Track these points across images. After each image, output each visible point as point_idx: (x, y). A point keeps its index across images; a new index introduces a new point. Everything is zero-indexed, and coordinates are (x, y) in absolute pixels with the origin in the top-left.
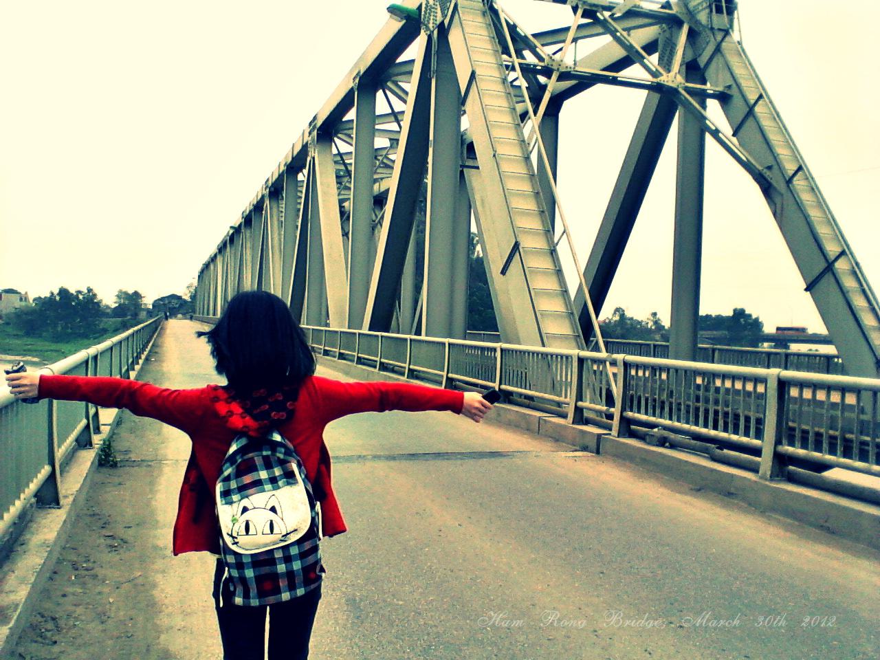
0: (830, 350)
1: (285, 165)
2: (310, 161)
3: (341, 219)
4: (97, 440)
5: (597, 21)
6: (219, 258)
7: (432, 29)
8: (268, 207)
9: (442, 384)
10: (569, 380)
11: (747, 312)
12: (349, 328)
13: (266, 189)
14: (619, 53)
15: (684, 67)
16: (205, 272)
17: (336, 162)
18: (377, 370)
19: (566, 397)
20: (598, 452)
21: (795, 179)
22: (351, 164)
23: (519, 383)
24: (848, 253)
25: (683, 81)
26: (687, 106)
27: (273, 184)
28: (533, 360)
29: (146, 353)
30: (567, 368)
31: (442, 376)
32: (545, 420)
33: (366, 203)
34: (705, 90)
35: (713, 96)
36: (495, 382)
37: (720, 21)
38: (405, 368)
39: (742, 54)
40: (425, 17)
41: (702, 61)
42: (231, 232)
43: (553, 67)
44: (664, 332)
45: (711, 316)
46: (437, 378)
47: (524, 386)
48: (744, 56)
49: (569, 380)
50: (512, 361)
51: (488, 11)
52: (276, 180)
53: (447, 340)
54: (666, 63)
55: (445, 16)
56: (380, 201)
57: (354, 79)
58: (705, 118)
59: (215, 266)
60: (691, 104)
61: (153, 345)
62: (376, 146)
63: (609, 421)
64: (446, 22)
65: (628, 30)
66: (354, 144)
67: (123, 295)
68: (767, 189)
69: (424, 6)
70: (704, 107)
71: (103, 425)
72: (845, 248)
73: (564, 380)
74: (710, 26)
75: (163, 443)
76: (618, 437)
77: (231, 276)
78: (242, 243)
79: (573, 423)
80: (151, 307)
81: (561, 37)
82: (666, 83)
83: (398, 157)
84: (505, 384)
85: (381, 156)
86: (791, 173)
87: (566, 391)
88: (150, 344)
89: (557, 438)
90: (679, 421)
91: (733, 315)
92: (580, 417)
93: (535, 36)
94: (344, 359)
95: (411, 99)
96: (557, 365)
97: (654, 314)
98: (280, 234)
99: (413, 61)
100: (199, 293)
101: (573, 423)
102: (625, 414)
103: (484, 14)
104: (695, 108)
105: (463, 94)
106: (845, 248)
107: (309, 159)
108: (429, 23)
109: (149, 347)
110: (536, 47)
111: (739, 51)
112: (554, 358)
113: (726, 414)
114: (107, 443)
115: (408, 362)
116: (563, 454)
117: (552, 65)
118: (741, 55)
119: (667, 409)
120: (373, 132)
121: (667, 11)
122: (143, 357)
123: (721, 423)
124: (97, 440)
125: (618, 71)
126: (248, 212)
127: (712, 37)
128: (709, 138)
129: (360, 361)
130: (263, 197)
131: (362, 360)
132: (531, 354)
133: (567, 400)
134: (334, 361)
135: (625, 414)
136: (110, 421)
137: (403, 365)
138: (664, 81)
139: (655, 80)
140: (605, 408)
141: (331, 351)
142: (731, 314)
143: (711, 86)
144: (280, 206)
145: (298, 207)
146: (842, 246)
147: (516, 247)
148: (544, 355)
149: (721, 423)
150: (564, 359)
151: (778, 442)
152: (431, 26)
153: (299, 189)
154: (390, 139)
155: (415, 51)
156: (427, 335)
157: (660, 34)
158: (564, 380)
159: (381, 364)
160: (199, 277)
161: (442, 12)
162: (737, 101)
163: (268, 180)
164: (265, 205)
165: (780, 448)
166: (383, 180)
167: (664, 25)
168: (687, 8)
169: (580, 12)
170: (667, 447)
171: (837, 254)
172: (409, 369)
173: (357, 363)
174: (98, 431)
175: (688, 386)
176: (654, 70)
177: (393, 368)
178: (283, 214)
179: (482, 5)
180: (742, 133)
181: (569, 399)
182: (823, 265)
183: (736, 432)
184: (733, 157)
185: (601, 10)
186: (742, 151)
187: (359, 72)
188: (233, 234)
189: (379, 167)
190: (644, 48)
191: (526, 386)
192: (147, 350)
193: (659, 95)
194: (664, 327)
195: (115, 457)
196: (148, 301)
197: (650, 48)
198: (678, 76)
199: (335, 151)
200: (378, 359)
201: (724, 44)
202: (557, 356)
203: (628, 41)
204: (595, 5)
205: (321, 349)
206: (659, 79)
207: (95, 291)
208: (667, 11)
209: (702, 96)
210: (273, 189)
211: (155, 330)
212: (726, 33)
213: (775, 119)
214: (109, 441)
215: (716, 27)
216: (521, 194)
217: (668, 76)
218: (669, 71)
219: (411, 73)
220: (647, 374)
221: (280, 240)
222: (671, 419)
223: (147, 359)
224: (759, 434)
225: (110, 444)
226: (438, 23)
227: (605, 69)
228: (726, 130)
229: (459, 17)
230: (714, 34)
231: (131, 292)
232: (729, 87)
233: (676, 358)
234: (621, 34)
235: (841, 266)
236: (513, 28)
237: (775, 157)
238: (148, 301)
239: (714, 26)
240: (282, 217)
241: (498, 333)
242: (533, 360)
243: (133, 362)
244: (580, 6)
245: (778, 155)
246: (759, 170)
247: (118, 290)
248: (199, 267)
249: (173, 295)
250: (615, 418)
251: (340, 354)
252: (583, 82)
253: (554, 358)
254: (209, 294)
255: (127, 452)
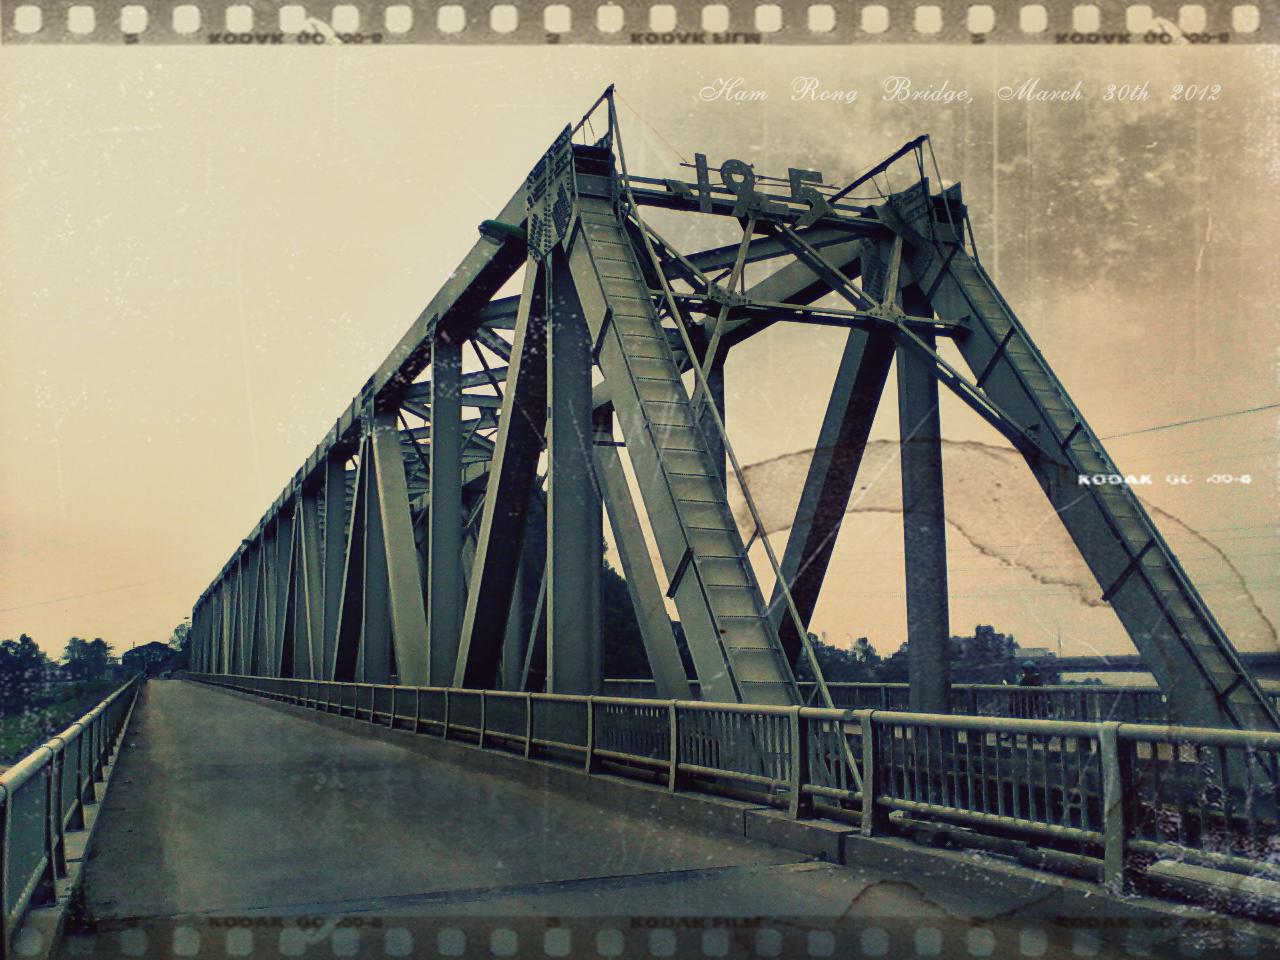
0: (1144, 680)
2: (365, 443)
4: (64, 888)
5: (774, 235)
7: (544, 253)
8: (301, 509)
10: (786, 750)
11: (996, 631)
12: (432, 685)
13: (297, 484)
14: (806, 277)
15: (900, 295)
19: (783, 778)
20: (842, 860)
21: (1072, 442)
22: (428, 445)
25: (903, 314)
26: (910, 346)
27: (307, 477)
29: (121, 735)
30: (782, 733)
32: (755, 816)
33: (454, 498)
36: (669, 759)
37: (943, 232)
41: (926, 286)
42: (245, 547)
43: (719, 301)
46: (577, 757)
47: (715, 764)
49: (786, 750)
50: (538, 707)
51: (624, 229)
52: (1014, 444)
54: (875, 287)
55: (562, 235)
56: (472, 493)
57: (429, 325)
58: (934, 360)
59: (220, 600)
60: (916, 344)
61: (130, 722)
62: (465, 417)
63: (857, 812)
64: (565, 245)
65: (817, 247)
67: (77, 645)
68: (1036, 459)
69: (530, 222)
70: (934, 347)
71: (69, 861)
73: (778, 751)
74: (931, 239)
76: (872, 835)
77: (244, 613)
78: (262, 566)
79: (798, 818)
80: (120, 662)
81: (728, 259)
82: (878, 317)
83: (497, 436)
84: (685, 762)
86: (1066, 434)
88: (127, 722)
89: (776, 842)
92: (808, 809)
94: (427, 732)
97: (864, 641)
98: (319, 550)
99: (517, 299)
101: (798, 818)
102: (879, 800)
103: (618, 231)
107: (362, 440)
108: (539, 246)
110: (693, 273)
111: (975, 270)
112: (761, 720)
113: (1008, 787)
115: (590, 744)
116: (792, 868)
117: (718, 298)
118: (979, 277)
119: (944, 790)
120: (462, 400)
121: (871, 220)
122: (119, 742)
124: (64, 888)
127: (936, 252)
128: (943, 389)
130: (293, 495)
131: (604, 762)
132: (730, 715)
134: (411, 736)
135: (879, 800)
136: (80, 853)
137: (523, 738)
138: (876, 314)
139: (863, 313)
140: (846, 792)
141: (405, 720)
142: (972, 634)
143: (940, 317)
145: (348, 508)
146: (1149, 534)
147: (689, 555)
148: (746, 716)
150: (768, 719)
151: (1128, 834)
152: (542, 249)
153: (348, 482)
154: (481, 409)
155: (517, 284)
156: (555, 692)
157: (861, 251)
158: (778, 751)
160: (194, 615)
161: (558, 230)
162: (979, 336)
163: (300, 472)
164: (296, 508)
165: (1133, 844)
167: (867, 239)
168: (899, 217)
169: (751, 225)
170: (948, 848)
171: (1144, 545)
174: (62, 873)
175: (947, 746)
176: (858, 296)
177: (504, 744)
178: (325, 520)
180: (988, 382)
181: (787, 780)
182: (1126, 561)
187: (437, 315)
188: (247, 551)
189: (467, 447)
190: (842, 269)
192: (123, 731)
194: (879, 657)
195: (92, 917)
197: (852, 270)
198: (895, 307)
199: (401, 427)
201: (953, 262)
203: (821, 261)
204: (773, 216)
205: (389, 718)
206: (869, 312)
207: (35, 640)
208: (871, 220)
209: (929, 333)
210: (307, 484)
211: (130, 701)
212: (957, 246)
213: (1035, 360)
215: (941, 240)
216: (690, 480)
217: (881, 308)
219: (514, 314)
221: (320, 556)
222: (952, 804)
223: (124, 745)
225: (82, 893)
226: (552, 245)
227: (788, 301)
228: (969, 376)
229: (584, 235)
230: (938, 249)
231: (90, 640)
232: (967, 319)
233: (921, 711)
235: (1150, 561)
236: (661, 248)
237: (1043, 414)
243: (105, 751)
244: (750, 217)
246: (1021, 432)
247: (70, 637)
251: (419, 724)
252: (751, 320)
253: (761, 720)
255: (108, 905)
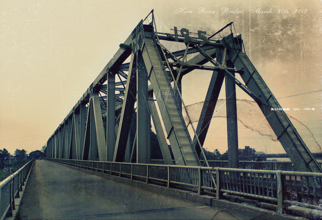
0: (287, 160)
1: (81, 102)
2: (90, 100)
3: (103, 120)
4: (14, 212)
6: (55, 136)
9: (146, 181)
10: (197, 178)
11: (250, 148)
12: (107, 161)
14: (202, 58)
16: (50, 142)
17: (100, 100)
18: (131, 180)
19: (196, 185)
21: (269, 100)
22: (106, 101)
23: (177, 180)
24: (291, 125)
27: (76, 108)
28: (182, 171)
29: (29, 174)
30: (196, 173)
31: (119, 173)
34: (234, 70)
35: (237, 72)
36: (168, 180)
37: (237, 47)
38: (131, 176)
39: (246, 57)
40: (133, 48)
42: (60, 126)
44: (221, 156)
45: (254, 151)
46: (144, 179)
48: (247, 58)
49: (197, 178)
53: (147, 164)
54: (220, 60)
55: (140, 47)
56: (118, 112)
57: (107, 70)
58: (235, 79)
59: (54, 139)
60: (230, 75)
61: (31, 170)
62: (116, 93)
64: (141, 50)
65: (205, 50)
66: (107, 93)
69: (132, 44)
70: (235, 76)
72: (290, 123)
73: (195, 178)
74: (234, 48)
75: (40, 211)
76: (219, 199)
79: (200, 194)
80: (29, 155)
81: (182, 53)
82: (220, 68)
83: (124, 98)
85: (117, 97)
86: (268, 98)
87: (196, 182)
88: (30, 170)
89: (195, 201)
90: (242, 192)
91: (245, 149)
92: (203, 193)
93: (173, 53)
95: (129, 78)
96: (192, 172)
97: (217, 150)
99: (129, 63)
100: (47, 150)
102: (221, 190)
103: (155, 46)
104: (232, 76)
105: (119, 75)
106: (290, 123)
107: (90, 99)
109: (30, 171)
110: (174, 57)
113: (253, 187)
114: (18, 214)
116: (198, 207)
117: (180, 63)
118: (246, 58)
119: (237, 187)
120: (115, 89)
121: (218, 44)
122: (28, 175)
123: (259, 192)
124: (14, 212)
125: (202, 65)
126: (66, 119)
129: (113, 174)
130: (72, 113)
133: (197, 186)
134: (102, 174)
136: (18, 204)
139: (217, 67)
141: (101, 170)
142: (244, 148)
144: (79, 116)
147: (172, 128)
148: (187, 169)
149: (259, 192)
150: (193, 170)
151: (284, 199)
152: (135, 51)
153: (86, 110)
154: (120, 91)
155: (129, 60)
156: (139, 163)
158: (195, 178)
159: (121, 174)
160: (47, 143)
162: (246, 73)
163: (74, 107)
164: (73, 116)
166: (117, 106)
167: (217, 48)
168: (226, 43)
169: (188, 45)
170: (238, 202)
171: (287, 126)
172: (148, 179)
173: (93, 170)
174: (14, 209)
176: (215, 63)
177: (126, 176)
179: (154, 43)
181: (197, 185)
182: (283, 130)
183: (250, 193)
184: (246, 92)
185: (196, 44)
186: (249, 90)
187: (109, 68)
188: (61, 127)
189: (116, 101)
190: (211, 56)
191: (180, 181)
192: (29, 173)
193: (218, 72)
194: (220, 154)
196: (28, 153)
197: (214, 56)
198: (225, 65)
199: (100, 96)
200: (131, 175)
202: (179, 168)
206: (218, 67)
207: (7, 150)
208: (218, 44)
209: (233, 72)
210: (76, 110)
212: (240, 50)
214: (19, 212)
216: (173, 109)
217: (221, 66)
218: (221, 64)
219: (128, 67)
220: (228, 174)
221: (79, 129)
222: (239, 191)
223: (30, 176)
224: (275, 196)
226: (138, 50)
227: (197, 64)
229: (146, 47)
231: (21, 150)
232: (243, 69)
234: (203, 52)
235: (289, 130)
236: (165, 51)
237: (262, 93)
238: (28, 153)
239: (235, 48)
240: (80, 120)
241: (163, 160)
242: (182, 171)
243: (25, 178)
244: (188, 43)
245: (263, 91)
246: (256, 97)
247: (16, 149)
248: (47, 140)
249: (37, 150)
250: (217, 192)
252: (188, 69)
254: (51, 150)
255: (26, 217)
